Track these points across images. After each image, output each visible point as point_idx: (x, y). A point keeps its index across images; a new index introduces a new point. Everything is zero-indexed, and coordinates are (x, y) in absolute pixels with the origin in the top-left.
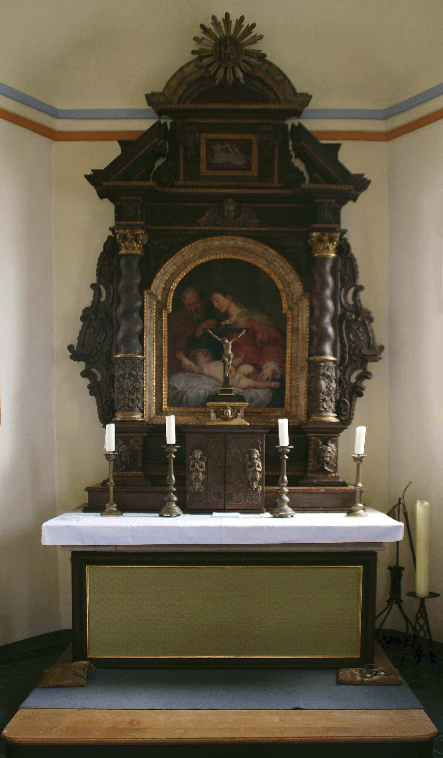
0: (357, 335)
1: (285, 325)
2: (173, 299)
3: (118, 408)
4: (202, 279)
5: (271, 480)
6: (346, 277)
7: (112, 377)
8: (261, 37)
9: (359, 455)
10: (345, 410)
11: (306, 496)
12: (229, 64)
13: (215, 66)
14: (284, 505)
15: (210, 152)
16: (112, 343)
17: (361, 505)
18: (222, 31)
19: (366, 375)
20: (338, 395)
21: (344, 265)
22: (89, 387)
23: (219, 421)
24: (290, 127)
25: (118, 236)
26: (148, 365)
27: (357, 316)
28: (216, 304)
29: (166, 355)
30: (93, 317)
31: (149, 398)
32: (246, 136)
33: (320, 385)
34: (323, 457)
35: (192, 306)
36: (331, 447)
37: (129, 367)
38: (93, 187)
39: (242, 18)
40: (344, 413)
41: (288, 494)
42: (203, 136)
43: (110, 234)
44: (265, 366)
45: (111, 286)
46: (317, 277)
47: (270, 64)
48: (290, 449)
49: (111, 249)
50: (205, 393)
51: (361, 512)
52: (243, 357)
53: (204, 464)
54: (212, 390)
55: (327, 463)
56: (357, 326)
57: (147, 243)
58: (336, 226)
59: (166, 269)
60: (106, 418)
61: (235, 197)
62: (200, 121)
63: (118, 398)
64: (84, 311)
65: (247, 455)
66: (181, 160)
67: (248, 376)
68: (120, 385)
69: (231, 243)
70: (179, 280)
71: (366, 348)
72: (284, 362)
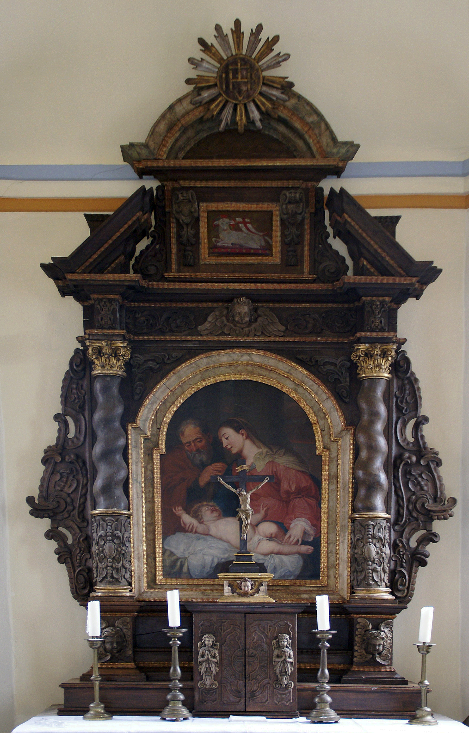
0: (419, 483)
1: (320, 470)
2: (167, 435)
3: (98, 579)
4: (206, 406)
5: (307, 674)
6: (404, 405)
7: (88, 539)
8: (287, 57)
9: (424, 643)
10: (403, 584)
11: (352, 696)
12: (240, 98)
13: (220, 102)
14: (325, 707)
15: (213, 230)
16: (86, 494)
17: (429, 710)
18: (230, 48)
19: (431, 538)
20: (392, 563)
21: (402, 389)
22: (57, 552)
23: (235, 598)
24: (326, 192)
25: (90, 349)
26: (136, 523)
27: (419, 458)
28: (225, 442)
29: (160, 510)
30: (59, 459)
31: (139, 566)
32: (265, 206)
33: (369, 550)
34: (375, 646)
35: (193, 444)
36: (384, 631)
37: (111, 526)
38: (51, 281)
39: (260, 28)
40: (401, 587)
41: (329, 692)
42: (203, 206)
43: (79, 346)
44: (292, 526)
45: (82, 417)
46: (364, 406)
47: (299, 97)
48: (333, 634)
49: (80, 365)
50: (213, 560)
51: (429, 718)
52: (263, 512)
53: (217, 652)
54: (222, 556)
55: (380, 654)
56: (418, 472)
57: (130, 359)
58: (392, 334)
59: (157, 395)
60: (83, 591)
61: (250, 295)
62: (198, 185)
63: (97, 567)
64: (46, 451)
65: (274, 641)
66: (173, 241)
67: (270, 538)
68: (101, 549)
69: (245, 358)
70: (175, 409)
71: (430, 501)
72: (319, 519)
